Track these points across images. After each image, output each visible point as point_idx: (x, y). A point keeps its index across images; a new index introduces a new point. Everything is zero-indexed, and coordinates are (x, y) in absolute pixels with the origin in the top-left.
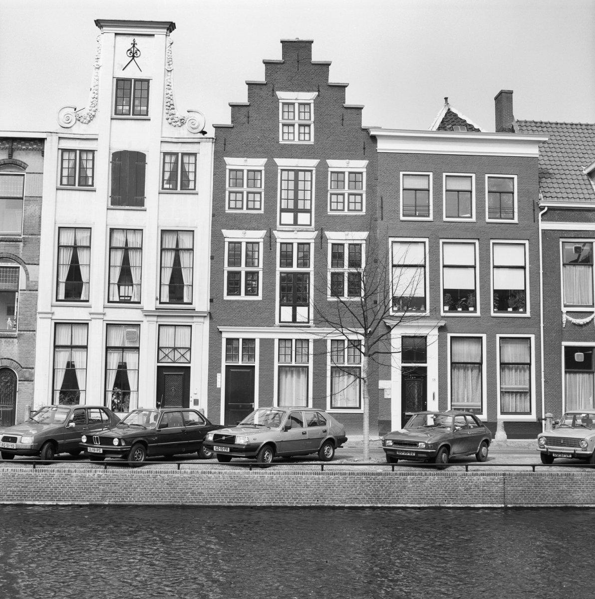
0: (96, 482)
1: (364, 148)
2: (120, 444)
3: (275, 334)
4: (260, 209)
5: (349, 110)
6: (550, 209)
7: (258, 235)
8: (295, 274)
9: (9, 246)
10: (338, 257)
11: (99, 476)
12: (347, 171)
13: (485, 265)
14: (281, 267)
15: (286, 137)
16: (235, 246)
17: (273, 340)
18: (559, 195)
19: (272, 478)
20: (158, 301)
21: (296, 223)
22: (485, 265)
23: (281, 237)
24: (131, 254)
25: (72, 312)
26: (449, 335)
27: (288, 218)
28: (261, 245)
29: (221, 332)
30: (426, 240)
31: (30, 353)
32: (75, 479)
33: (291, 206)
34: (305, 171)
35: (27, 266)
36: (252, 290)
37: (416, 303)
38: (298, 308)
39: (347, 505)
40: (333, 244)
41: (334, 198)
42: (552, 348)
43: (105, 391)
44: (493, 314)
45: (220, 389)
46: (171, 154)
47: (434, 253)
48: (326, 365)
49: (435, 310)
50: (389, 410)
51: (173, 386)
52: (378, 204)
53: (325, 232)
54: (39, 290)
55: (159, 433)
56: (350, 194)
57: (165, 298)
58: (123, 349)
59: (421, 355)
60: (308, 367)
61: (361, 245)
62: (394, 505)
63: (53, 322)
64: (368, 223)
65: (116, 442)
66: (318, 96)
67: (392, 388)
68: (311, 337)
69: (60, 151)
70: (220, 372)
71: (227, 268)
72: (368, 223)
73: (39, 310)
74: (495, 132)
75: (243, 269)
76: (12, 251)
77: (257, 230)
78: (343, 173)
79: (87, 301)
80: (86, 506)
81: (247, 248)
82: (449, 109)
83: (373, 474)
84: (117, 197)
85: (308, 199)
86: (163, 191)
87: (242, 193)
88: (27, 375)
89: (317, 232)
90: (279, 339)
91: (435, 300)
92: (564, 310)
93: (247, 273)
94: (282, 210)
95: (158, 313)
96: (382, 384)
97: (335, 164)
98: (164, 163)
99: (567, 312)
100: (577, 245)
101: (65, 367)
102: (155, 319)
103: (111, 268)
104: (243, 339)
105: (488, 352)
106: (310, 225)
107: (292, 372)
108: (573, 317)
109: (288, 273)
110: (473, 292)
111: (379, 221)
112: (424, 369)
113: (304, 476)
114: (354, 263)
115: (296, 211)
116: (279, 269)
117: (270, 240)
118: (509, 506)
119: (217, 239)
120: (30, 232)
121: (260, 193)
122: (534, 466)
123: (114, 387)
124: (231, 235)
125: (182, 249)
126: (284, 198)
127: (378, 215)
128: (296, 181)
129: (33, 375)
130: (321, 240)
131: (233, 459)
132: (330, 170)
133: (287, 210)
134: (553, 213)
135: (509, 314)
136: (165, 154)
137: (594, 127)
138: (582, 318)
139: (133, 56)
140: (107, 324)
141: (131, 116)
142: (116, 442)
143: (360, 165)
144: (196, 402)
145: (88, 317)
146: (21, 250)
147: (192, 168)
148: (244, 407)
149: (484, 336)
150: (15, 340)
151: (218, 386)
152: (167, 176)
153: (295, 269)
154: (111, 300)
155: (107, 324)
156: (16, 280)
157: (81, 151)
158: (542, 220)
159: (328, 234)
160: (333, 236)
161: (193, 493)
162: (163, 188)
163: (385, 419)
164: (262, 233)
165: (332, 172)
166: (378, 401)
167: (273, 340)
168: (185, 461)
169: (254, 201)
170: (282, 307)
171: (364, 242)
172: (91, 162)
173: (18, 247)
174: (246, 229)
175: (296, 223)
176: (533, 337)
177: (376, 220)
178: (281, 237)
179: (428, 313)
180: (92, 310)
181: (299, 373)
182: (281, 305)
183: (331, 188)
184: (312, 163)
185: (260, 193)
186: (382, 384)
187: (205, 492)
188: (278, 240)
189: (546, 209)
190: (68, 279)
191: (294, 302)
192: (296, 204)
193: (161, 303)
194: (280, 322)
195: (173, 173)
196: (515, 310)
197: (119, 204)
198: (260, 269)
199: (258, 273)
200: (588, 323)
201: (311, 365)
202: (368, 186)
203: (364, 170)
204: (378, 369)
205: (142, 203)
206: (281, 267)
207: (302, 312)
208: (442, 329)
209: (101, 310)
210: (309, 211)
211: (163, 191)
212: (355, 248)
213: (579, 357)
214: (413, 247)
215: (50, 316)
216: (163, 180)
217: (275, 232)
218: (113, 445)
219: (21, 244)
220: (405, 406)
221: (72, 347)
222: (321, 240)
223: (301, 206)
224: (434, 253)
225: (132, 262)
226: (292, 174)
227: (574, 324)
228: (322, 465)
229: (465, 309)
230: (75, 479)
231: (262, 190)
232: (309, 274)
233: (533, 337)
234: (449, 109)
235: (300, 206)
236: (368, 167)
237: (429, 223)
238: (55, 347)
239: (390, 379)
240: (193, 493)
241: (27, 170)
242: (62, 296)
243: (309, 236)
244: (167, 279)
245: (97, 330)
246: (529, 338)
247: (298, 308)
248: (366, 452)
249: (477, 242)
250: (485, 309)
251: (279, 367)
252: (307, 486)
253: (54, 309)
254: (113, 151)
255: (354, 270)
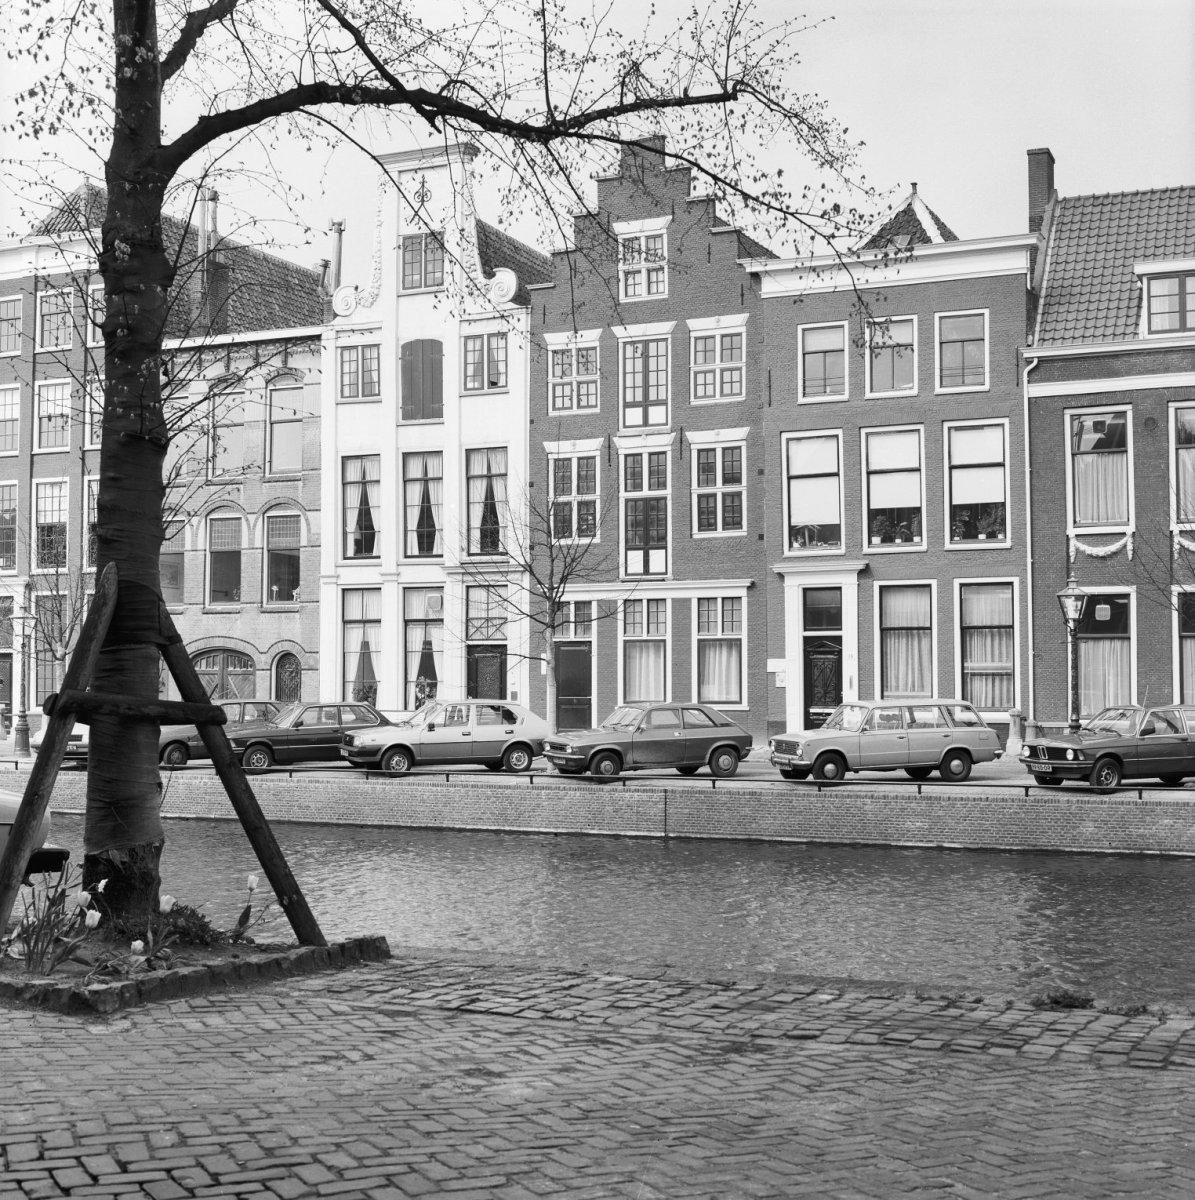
0: (202, 791)
1: (742, 295)
2: (1076, 758)
3: (616, 593)
4: (596, 406)
5: (718, 237)
6: (1041, 360)
7: (591, 446)
8: (646, 500)
9: (287, 487)
10: (707, 469)
11: (205, 783)
12: (718, 333)
13: (938, 466)
15: (637, 291)
16: (563, 464)
17: (689, 600)
18: (1069, 334)
19: (384, 789)
20: (465, 553)
21: (646, 423)
22: (938, 466)
23: (624, 445)
24: (431, 485)
25: (360, 573)
26: (877, 584)
27: (634, 416)
28: (598, 460)
30: (839, 432)
31: (313, 630)
32: (181, 787)
34: (657, 341)
35: (308, 513)
36: (732, 522)
37: (827, 534)
38: (651, 552)
39: (468, 827)
40: (699, 451)
42: (1046, 601)
43: (344, 683)
44: (948, 546)
46: (475, 337)
47: (853, 453)
48: (616, 638)
49: (855, 545)
50: (783, 705)
51: (488, 671)
52: (764, 380)
53: (687, 433)
55: (1142, 743)
56: (723, 371)
57: (475, 548)
58: (426, 622)
59: (834, 618)
60: (740, 640)
61: (740, 448)
62: (525, 829)
63: (401, 586)
64: (746, 414)
65: (1070, 755)
66: (673, 220)
67: (789, 671)
68: (669, 595)
69: (339, 351)
71: (696, 490)
72: (746, 414)
73: (323, 573)
74: (1027, 231)
75: (719, 488)
76: (290, 494)
77: (590, 437)
78: (713, 337)
79: (441, 556)
80: (192, 819)
82: (910, 204)
83: (500, 787)
84: (409, 407)
85: (663, 384)
86: (467, 392)
87: (713, 371)
88: (312, 662)
89: (674, 434)
90: (699, 599)
91: (854, 529)
92: (1071, 531)
93: (580, 504)
94: (627, 405)
95: (464, 569)
96: (773, 665)
97: (699, 326)
98: (466, 351)
99: (1181, 532)
100: (1099, 418)
101: (358, 649)
102: (460, 577)
103: (471, 506)
104: (576, 603)
105: (939, 610)
106: (667, 424)
107: (721, 646)
108: (1089, 545)
109: (636, 500)
110: (918, 510)
111: (766, 408)
112: (838, 640)
113: (420, 788)
114: (731, 478)
115: (646, 404)
116: (623, 495)
117: (609, 449)
118: (671, 835)
119: (537, 455)
120: (310, 467)
121: (740, 369)
122: (1027, 788)
123: (419, 676)
124: (556, 449)
125: (432, 479)
126: (630, 385)
127: (765, 398)
128: (646, 356)
129: (317, 661)
130: (681, 444)
131: (1065, 783)
132: (693, 334)
133: (634, 405)
134: (1045, 369)
135: (982, 543)
136: (467, 338)
137: (1193, 193)
138: (1105, 544)
139: (423, 201)
140: (405, 588)
141: (423, 289)
142: (1070, 755)
143: (736, 322)
144: (514, 696)
145: (379, 579)
146: (300, 492)
147: (502, 356)
148: (579, 702)
149: (934, 583)
150: (297, 615)
152: (471, 370)
153: (646, 493)
154: (409, 554)
155: (405, 588)
156: (297, 534)
157: (364, 347)
158: (1029, 382)
159: (691, 436)
160: (698, 439)
161: (300, 807)
162: (466, 389)
163: (778, 719)
165: (696, 339)
166: (764, 689)
167: (689, 600)
168: (304, 765)
169: (732, 382)
170: (629, 552)
172: (376, 361)
173: (296, 488)
174: (576, 439)
175: (646, 423)
176: (1016, 581)
177: (761, 407)
178: (624, 445)
179: (842, 550)
180: (383, 570)
181: (730, 647)
182: (627, 549)
183: (695, 362)
184: (664, 328)
185: (740, 369)
186: (773, 665)
187: (312, 805)
189: (1035, 362)
190: (420, 525)
191: (646, 543)
192: (646, 394)
193: (469, 555)
194: (626, 574)
195: (479, 365)
196: (992, 536)
197: (412, 418)
198: (596, 496)
199: (595, 502)
200: (1115, 554)
201: (669, 638)
202: (748, 355)
203: (743, 330)
204: (766, 642)
205: (440, 415)
207: (657, 558)
208: (864, 573)
209: (393, 569)
210: (664, 403)
211: (467, 392)
212: (586, 462)
213: (1103, 612)
214: (987, 432)
215: (334, 580)
216: (466, 377)
217: (615, 439)
218: (1067, 759)
219: (300, 483)
220: (809, 700)
221: (365, 622)
222: (681, 444)
224: (853, 453)
225: (498, 495)
227: (1091, 556)
228: (531, 777)
229: (908, 539)
230: (181, 787)
231: (742, 364)
232: (665, 499)
233: (1016, 581)
234: (910, 204)
235: (652, 396)
236: (750, 323)
237: (842, 405)
238: (345, 622)
239: (784, 657)
240: (300, 807)
241: (306, 381)
242: (351, 552)
243: (664, 442)
244: (413, 524)
245: (391, 597)
246: (929, 586)
247: (651, 552)
249: (864, 432)
250: (936, 538)
251: (625, 642)
252: (424, 801)
253: (341, 571)
254: (402, 343)
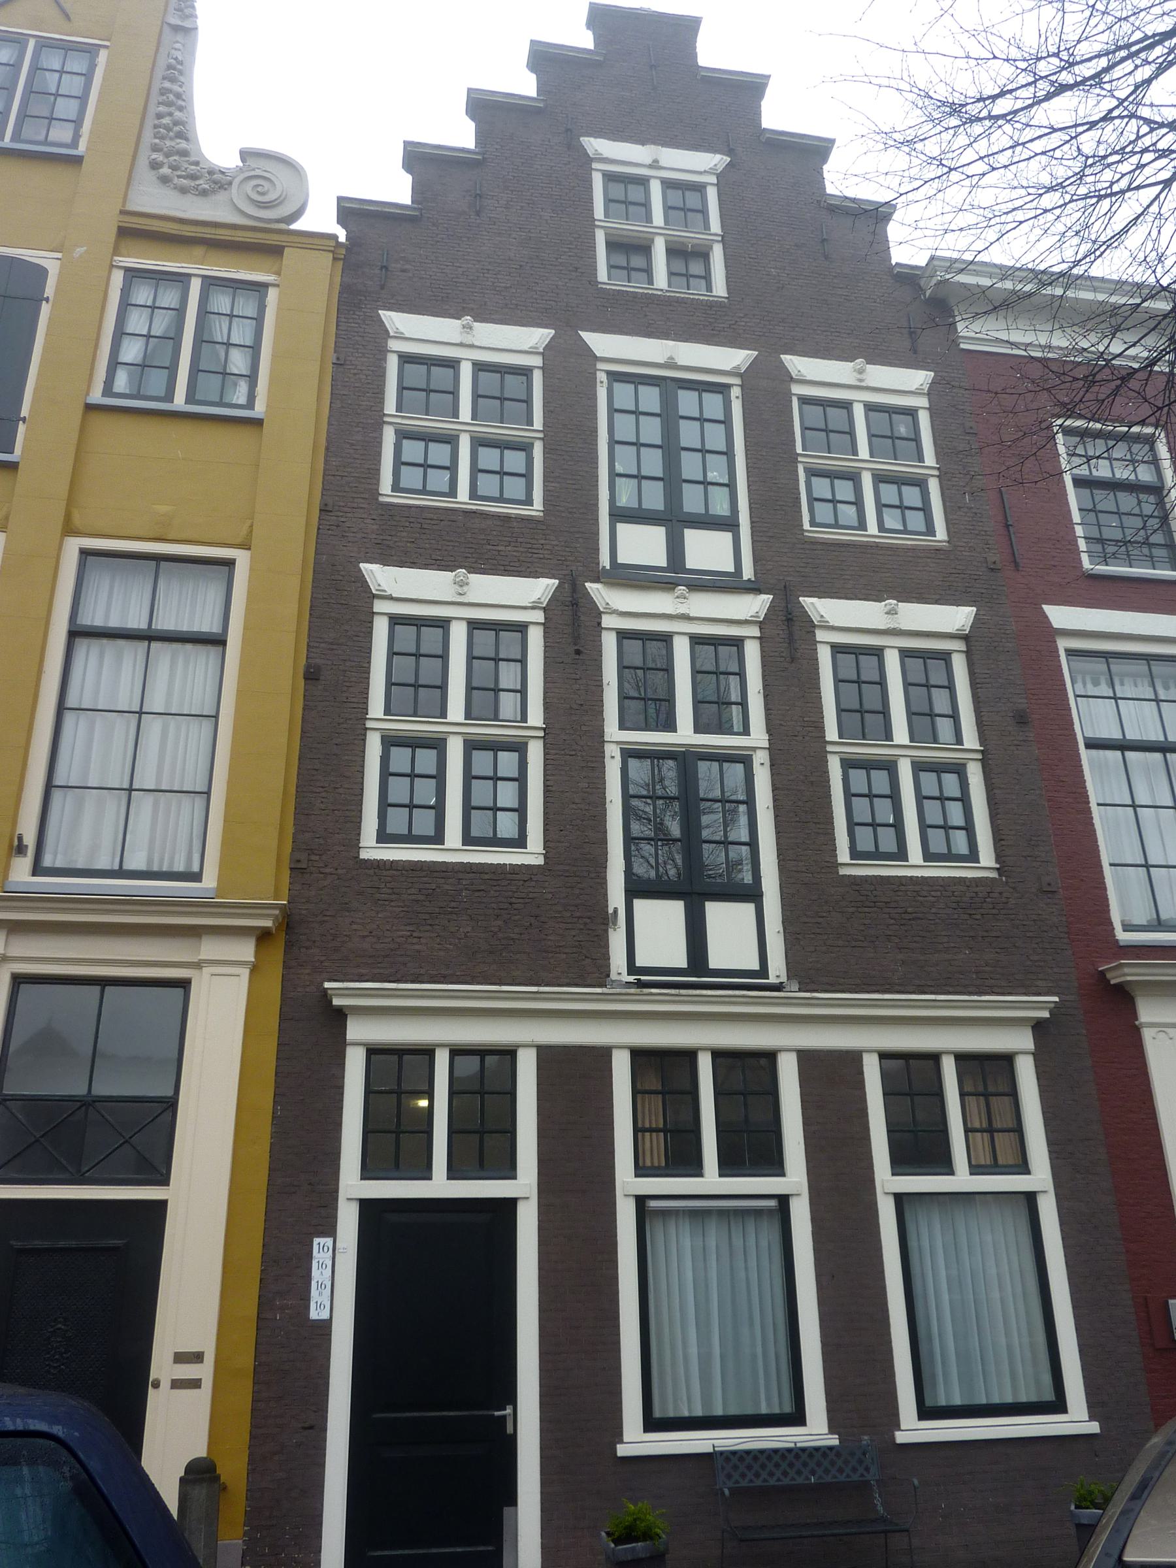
14: (622, 726)
29: (340, 1016)
33: (654, 497)
41: (822, 487)
45: (324, 1328)
54: (114, 230)
70: (330, 1230)
81: (385, 760)
94: (620, 515)
151: (317, 1313)
164: (541, 588)
171: (960, 645)
188: (608, 621)
194: (632, 968)
206: (622, 726)
210: (729, 524)
223: (692, 500)
226: (650, 398)
236: (933, 392)
248: (1116, 348)
255: (834, 1458)
